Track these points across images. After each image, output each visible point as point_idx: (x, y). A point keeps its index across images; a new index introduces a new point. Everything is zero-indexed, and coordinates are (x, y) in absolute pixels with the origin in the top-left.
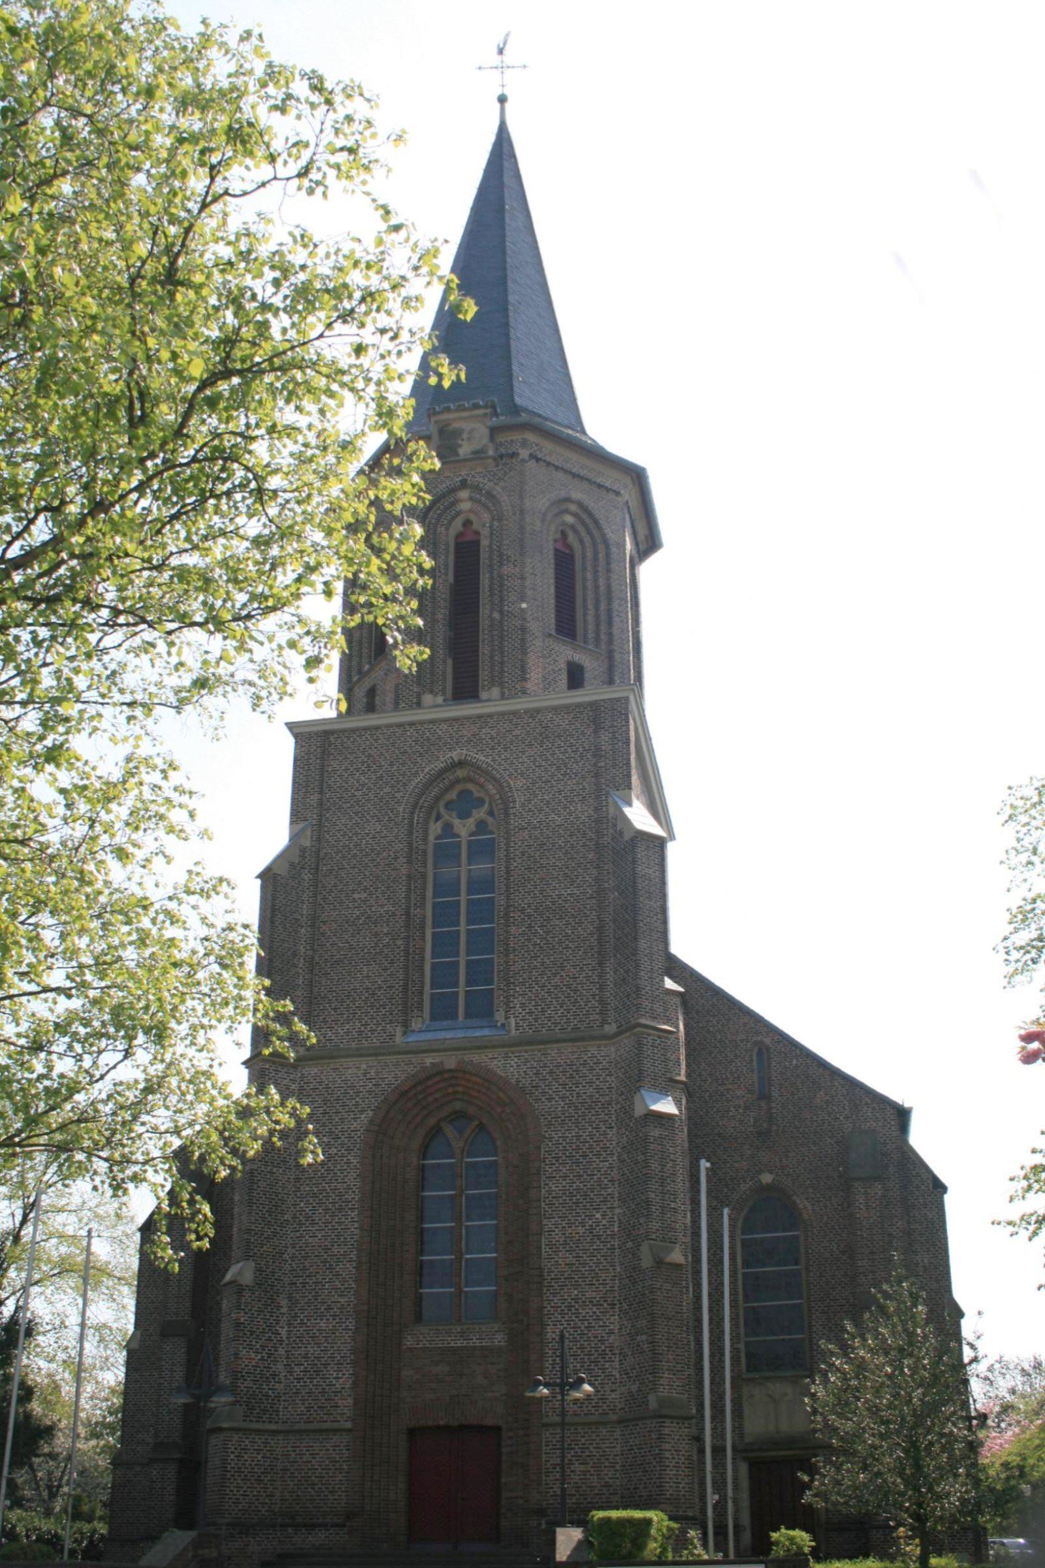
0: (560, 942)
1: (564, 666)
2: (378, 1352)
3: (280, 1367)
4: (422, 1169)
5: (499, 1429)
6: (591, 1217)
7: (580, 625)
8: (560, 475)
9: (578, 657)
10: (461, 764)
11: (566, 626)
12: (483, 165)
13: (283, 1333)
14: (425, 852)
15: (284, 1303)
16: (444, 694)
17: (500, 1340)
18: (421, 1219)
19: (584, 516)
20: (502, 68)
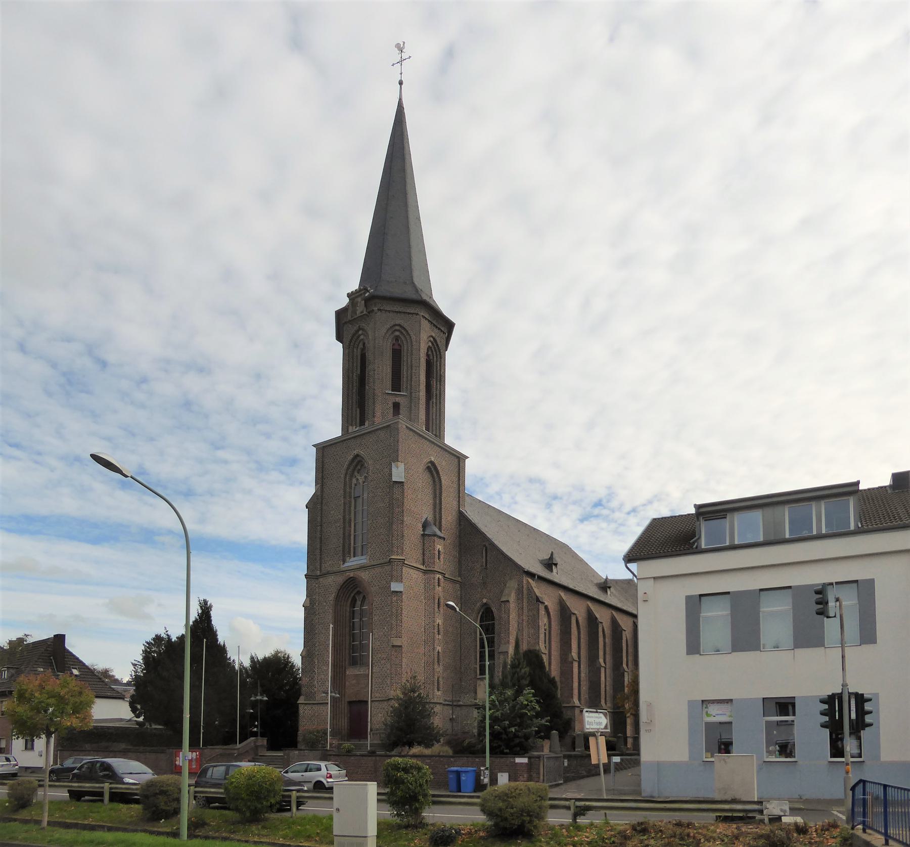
10: (358, 455)
11: (396, 385)
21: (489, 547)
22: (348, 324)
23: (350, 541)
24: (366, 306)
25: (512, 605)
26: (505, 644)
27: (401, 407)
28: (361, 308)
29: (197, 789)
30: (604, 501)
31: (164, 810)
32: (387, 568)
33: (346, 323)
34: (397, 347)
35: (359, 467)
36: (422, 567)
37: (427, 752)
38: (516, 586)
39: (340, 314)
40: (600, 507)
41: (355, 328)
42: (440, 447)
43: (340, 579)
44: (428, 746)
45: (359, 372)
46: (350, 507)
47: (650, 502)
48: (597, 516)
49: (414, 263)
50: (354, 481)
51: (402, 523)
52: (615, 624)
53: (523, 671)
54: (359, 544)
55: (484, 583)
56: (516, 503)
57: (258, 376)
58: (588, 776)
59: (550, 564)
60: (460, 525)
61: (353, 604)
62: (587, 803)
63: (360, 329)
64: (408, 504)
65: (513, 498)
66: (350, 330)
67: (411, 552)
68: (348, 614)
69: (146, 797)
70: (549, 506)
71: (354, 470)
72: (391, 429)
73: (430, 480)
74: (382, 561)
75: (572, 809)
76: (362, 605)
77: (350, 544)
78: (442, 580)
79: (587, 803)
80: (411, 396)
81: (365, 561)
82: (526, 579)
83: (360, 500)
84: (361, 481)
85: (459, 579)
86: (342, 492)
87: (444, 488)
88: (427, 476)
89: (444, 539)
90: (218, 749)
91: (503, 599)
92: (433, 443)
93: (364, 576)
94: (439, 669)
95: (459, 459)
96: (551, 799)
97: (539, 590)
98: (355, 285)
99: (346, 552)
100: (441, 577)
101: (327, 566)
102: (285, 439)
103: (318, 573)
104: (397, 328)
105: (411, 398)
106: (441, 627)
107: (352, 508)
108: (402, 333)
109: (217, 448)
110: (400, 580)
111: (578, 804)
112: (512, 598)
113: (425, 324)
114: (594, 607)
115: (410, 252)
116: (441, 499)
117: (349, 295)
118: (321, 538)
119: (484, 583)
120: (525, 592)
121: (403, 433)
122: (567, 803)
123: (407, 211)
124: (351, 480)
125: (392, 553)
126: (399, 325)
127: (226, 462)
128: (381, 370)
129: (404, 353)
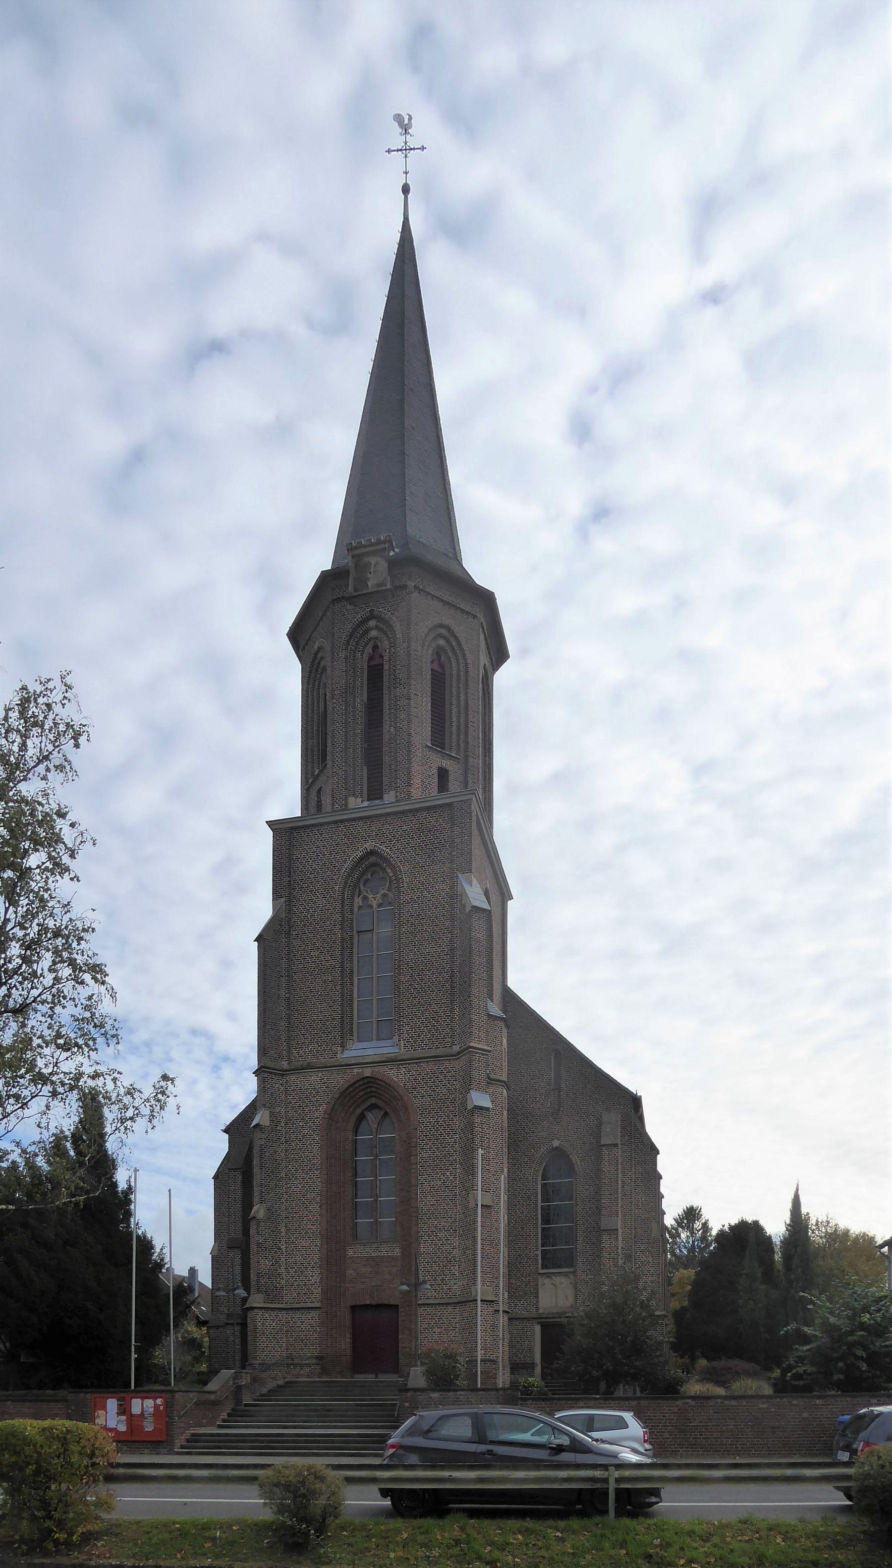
0: (429, 987)
1: (435, 771)
2: (333, 1262)
3: (283, 1269)
5: (397, 1306)
6: (444, 1174)
7: (447, 740)
9: (446, 763)
10: (372, 853)
11: (439, 740)
12: (370, 366)
13: (283, 1248)
14: (352, 920)
15: (283, 1229)
16: (362, 797)
17: (397, 1252)
18: (356, 1175)
19: (452, 639)
20: (406, 150)
27: (451, 778)
43: (340, 1080)
50: (358, 901)
56: (171, 1060)
65: (167, 1053)
70: (216, 1068)
71: (359, 879)
80: (466, 762)
93: (396, 1076)
103: (285, 1065)
104: (443, 631)
108: (448, 641)
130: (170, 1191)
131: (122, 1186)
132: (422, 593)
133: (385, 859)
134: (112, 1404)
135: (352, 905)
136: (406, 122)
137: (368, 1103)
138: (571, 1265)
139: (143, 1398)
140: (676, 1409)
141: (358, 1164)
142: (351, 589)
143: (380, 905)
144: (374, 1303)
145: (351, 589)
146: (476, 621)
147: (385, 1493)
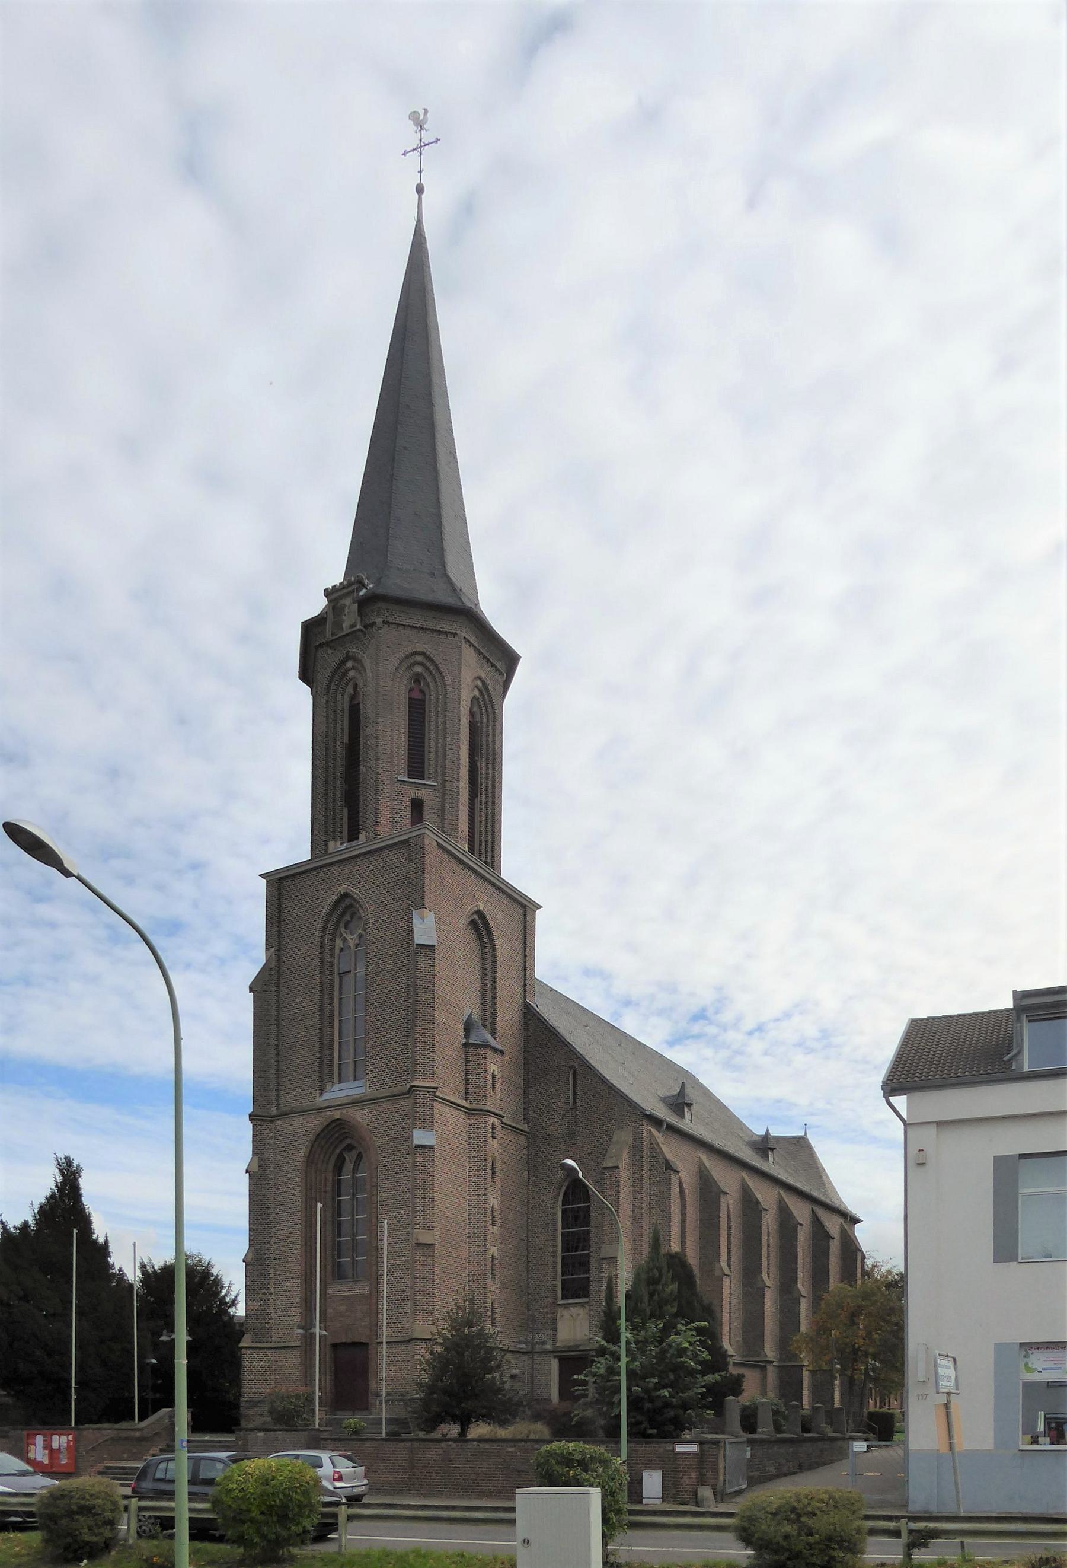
1: (408, 804)
3: (271, 1309)
4: (339, 1201)
8: (409, 632)
10: (345, 896)
11: (416, 768)
13: (272, 1288)
14: (332, 964)
15: (272, 1271)
16: (341, 839)
21: (579, 1069)
22: (325, 651)
23: (332, 1053)
24: (360, 612)
25: (624, 1175)
26: (611, 1243)
27: (426, 807)
28: (350, 618)
29: (144, 1503)
30: (710, 1013)
31: (87, 1543)
32: (406, 1104)
33: (321, 645)
34: (416, 695)
35: (347, 917)
36: (463, 1103)
37: (502, 1433)
38: (630, 1141)
39: (310, 629)
40: (702, 1022)
41: (339, 656)
42: (493, 885)
43: (316, 1123)
44: (503, 1423)
45: (346, 740)
46: (332, 991)
47: (787, 1015)
48: (697, 1037)
49: (446, 537)
50: (339, 943)
51: (432, 1021)
52: (784, 1211)
53: (668, 1290)
54: (349, 1059)
55: (572, 1135)
57: (114, 773)
58: (777, 1476)
59: (679, 1104)
60: (527, 1029)
61: (339, 1169)
62: (932, 1525)
63: (348, 658)
64: (442, 989)
66: (329, 659)
67: (445, 1073)
68: (329, 1186)
69: (52, 1518)
71: (338, 922)
72: (409, 848)
73: (476, 946)
74: (396, 1090)
75: (904, 1534)
76: (355, 1170)
77: (332, 1059)
78: (499, 1128)
79: (932, 1525)
81: (362, 1090)
82: (648, 1129)
83: (349, 979)
84: (351, 944)
85: (525, 1127)
86: (317, 962)
87: (500, 959)
88: (470, 937)
89: (502, 1053)
90: (107, 1430)
91: (608, 1163)
92: (483, 877)
93: (361, 1117)
94: (494, 1287)
95: (525, 909)
96: (867, 1517)
97: (670, 1149)
98: (336, 576)
99: (326, 1072)
100: (496, 1122)
101: (290, 1099)
102: (161, 887)
103: (274, 1111)
104: (419, 658)
105: (445, 792)
106: (497, 1212)
107: (336, 993)
109: (39, 900)
110: (428, 1124)
111: (914, 1526)
112: (624, 1162)
113: (469, 655)
114: (753, 1183)
115: (439, 516)
116: (494, 981)
117: (328, 593)
118: (277, 1046)
119: (572, 1135)
120: (646, 1152)
121: (432, 855)
122: (891, 1525)
123: (433, 437)
124: (333, 939)
125: (415, 1074)
126: (423, 654)
127: (53, 925)
128: (388, 735)
129: (431, 707)
130: (134, 1244)
131: (101, 1240)
132: (392, 626)
133: (355, 900)
134: (39, 1439)
135: (332, 948)
136: (422, 117)
137: (344, 1144)
138: (587, 1295)
139: (60, 1435)
140: (441, 1451)
141: (343, 1205)
142: (328, 634)
143: (357, 946)
144: (349, 1341)
145: (328, 634)
146: (457, 638)
147: (746, 1537)
